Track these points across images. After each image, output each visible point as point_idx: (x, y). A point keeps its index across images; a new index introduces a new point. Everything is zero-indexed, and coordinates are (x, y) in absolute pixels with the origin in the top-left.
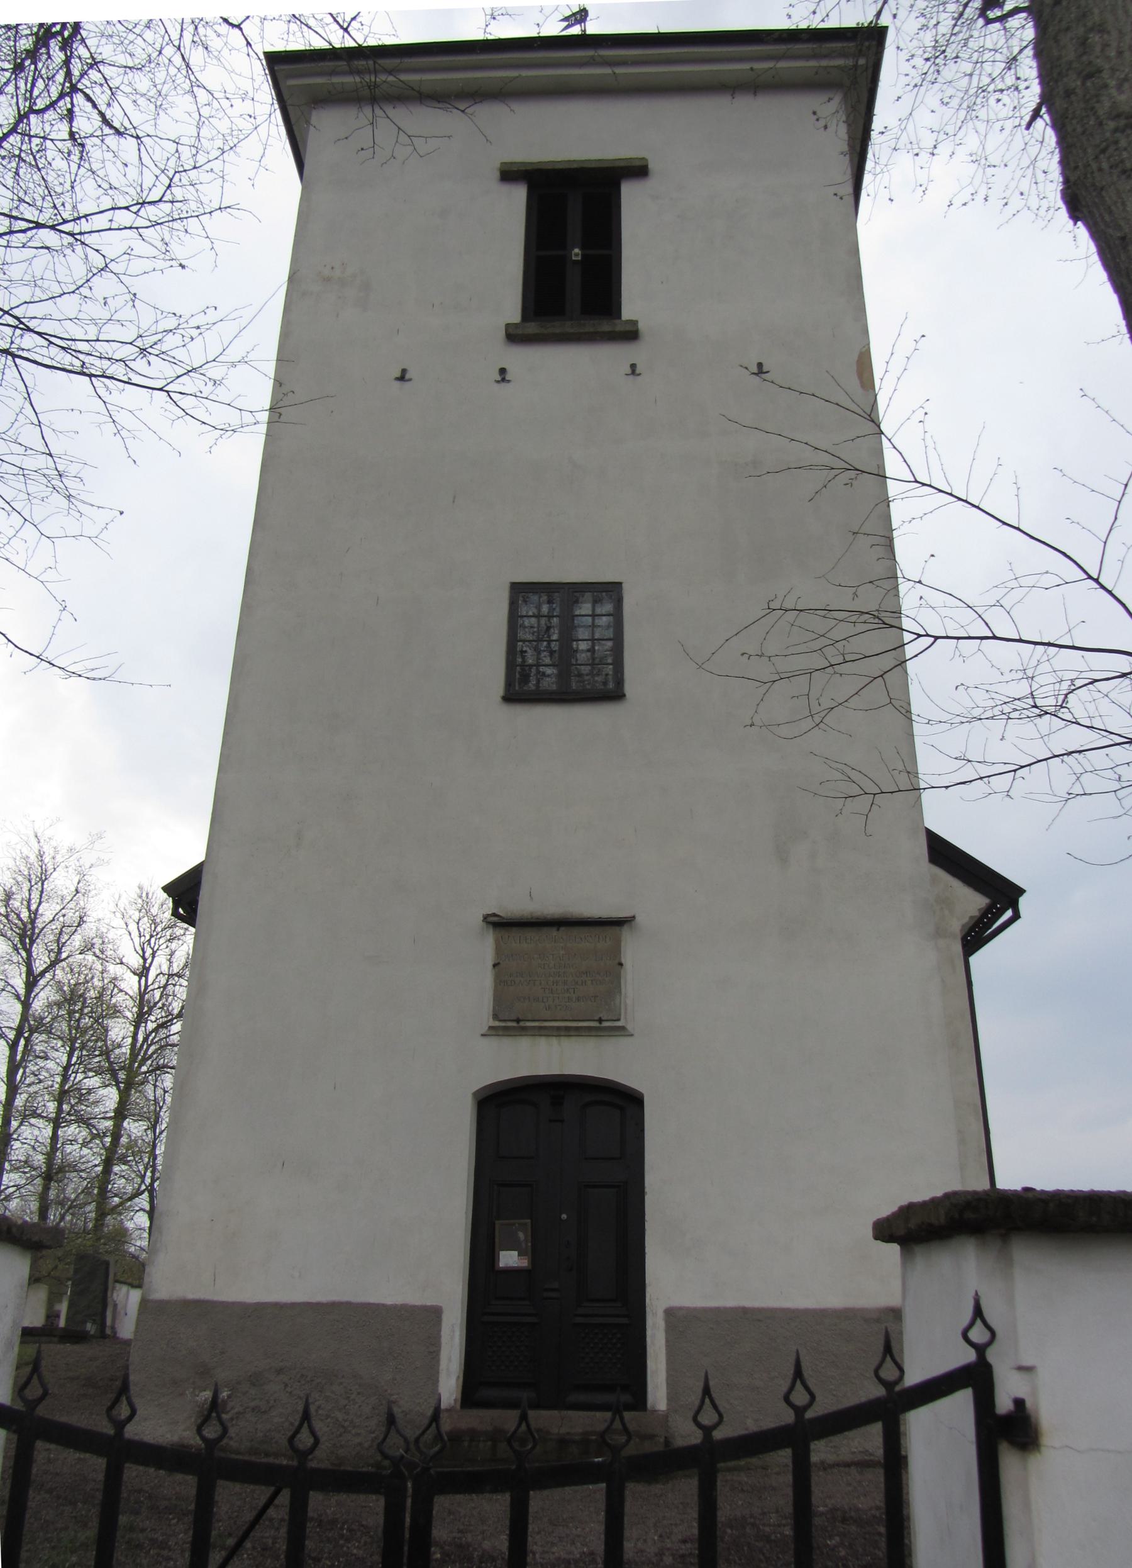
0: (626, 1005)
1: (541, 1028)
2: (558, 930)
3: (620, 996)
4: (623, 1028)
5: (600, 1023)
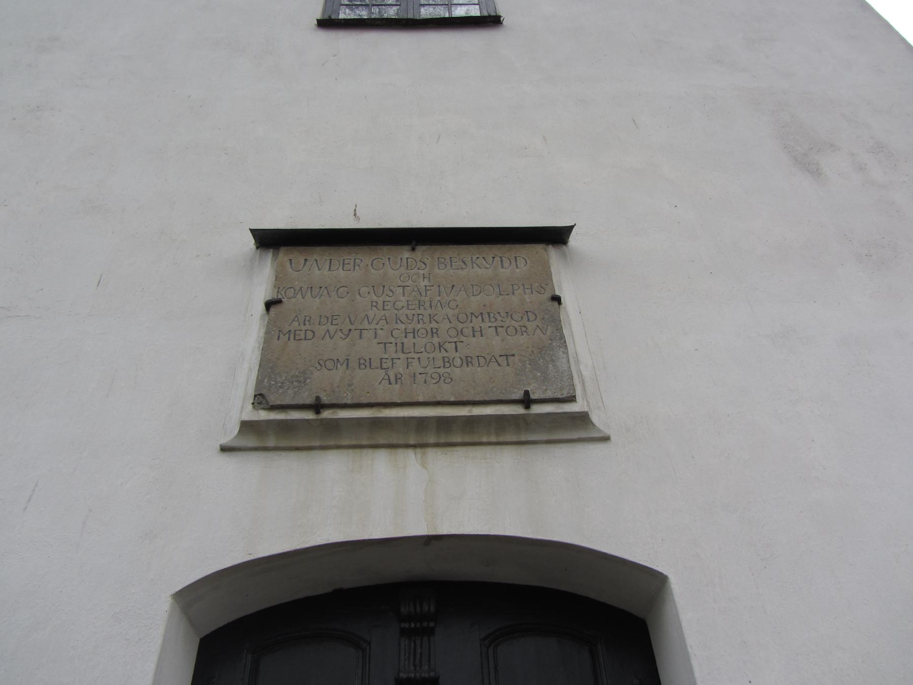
0: (581, 375)
1: (376, 423)
2: (413, 249)
3: (566, 353)
4: (583, 419)
5: (527, 407)
